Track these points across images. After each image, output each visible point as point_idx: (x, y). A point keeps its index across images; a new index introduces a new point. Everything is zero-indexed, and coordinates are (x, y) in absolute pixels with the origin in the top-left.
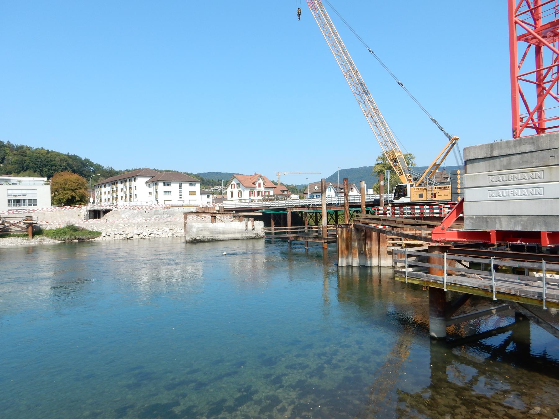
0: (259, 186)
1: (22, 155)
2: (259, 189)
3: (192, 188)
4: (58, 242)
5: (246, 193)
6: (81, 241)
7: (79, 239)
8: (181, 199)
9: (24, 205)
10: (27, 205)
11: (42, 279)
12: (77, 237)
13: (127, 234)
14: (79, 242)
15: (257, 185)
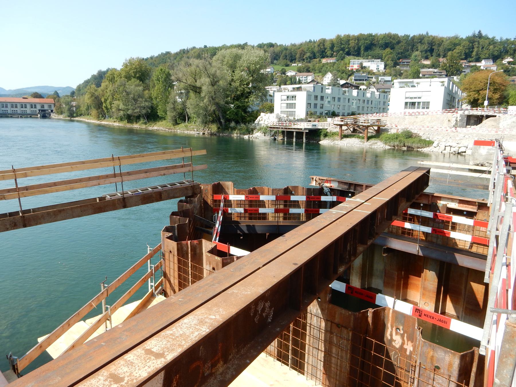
4: (387, 147)
6: (410, 149)
7: (408, 147)
9: (418, 108)
10: (421, 108)
12: (406, 144)
13: (460, 148)
14: (408, 150)
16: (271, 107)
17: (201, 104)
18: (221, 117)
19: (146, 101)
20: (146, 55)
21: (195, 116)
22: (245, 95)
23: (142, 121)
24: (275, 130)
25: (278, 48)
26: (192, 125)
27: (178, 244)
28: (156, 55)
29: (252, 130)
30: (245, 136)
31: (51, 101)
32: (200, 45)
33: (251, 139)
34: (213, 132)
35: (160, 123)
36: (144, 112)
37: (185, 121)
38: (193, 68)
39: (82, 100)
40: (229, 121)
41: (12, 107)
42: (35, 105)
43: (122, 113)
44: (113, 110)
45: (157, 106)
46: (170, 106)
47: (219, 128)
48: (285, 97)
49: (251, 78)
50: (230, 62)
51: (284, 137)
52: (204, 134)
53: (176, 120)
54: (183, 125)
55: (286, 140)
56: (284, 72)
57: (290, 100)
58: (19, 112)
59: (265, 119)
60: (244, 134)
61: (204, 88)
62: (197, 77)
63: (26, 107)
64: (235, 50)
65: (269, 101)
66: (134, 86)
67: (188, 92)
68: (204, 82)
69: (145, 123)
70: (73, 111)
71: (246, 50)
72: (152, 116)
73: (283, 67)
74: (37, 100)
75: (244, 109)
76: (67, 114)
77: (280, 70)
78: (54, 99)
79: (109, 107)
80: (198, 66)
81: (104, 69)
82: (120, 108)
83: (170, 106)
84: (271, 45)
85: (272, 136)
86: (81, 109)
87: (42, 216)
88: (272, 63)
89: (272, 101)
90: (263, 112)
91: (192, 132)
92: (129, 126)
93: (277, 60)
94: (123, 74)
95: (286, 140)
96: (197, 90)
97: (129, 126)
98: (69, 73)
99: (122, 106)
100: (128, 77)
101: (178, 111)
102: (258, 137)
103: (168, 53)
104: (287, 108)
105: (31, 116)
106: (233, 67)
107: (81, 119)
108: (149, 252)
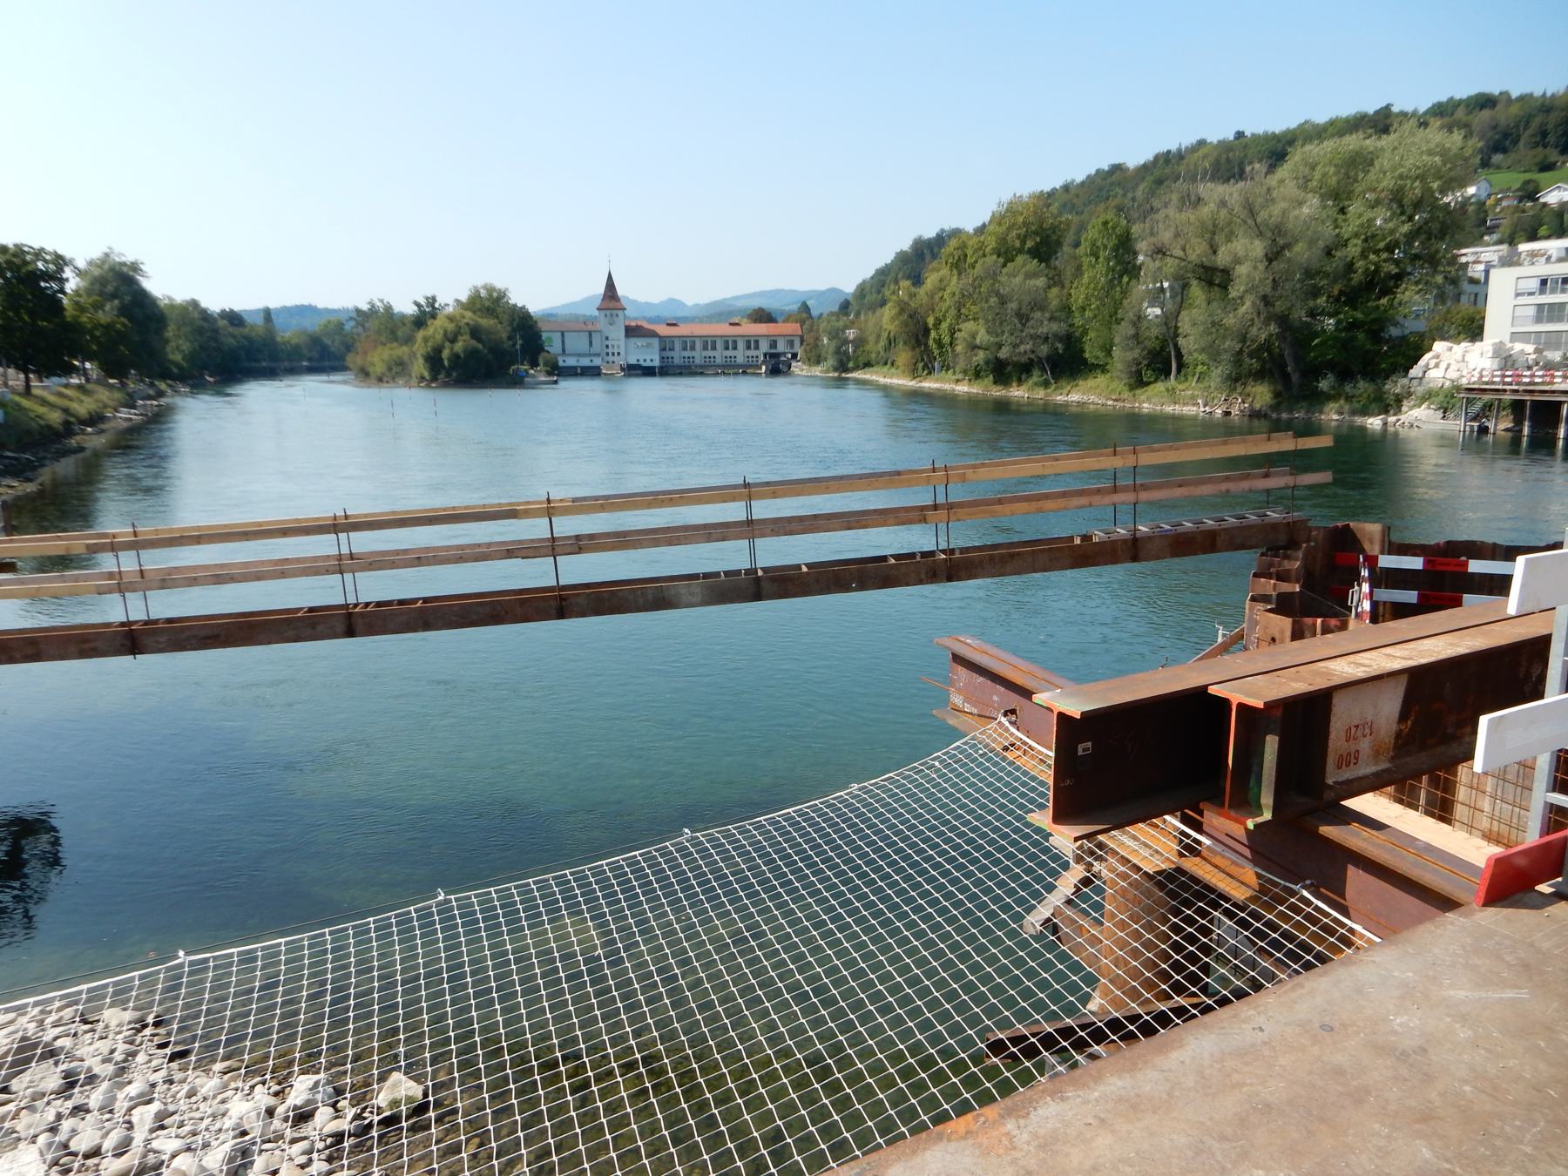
16: (1472, 320)
17: (1230, 320)
18: (1289, 360)
19: (1052, 319)
20: (1051, 181)
21: (1202, 357)
22: (1383, 285)
23: (1036, 376)
24: (1487, 397)
25: (1514, 110)
26: (1190, 387)
27: (1294, 623)
28: (1079, 178)
29: (1399, 401)
30: (1371, 420)
31: (793, 328)
32: (1219, 131)
33: (1391, 429)
34: (1257, 406)
35: (1091, 382)
36: (1044, 350)
37: (1167, 374)
38: (1206, 211)
39: (871, 324)
40: (1314, 372)
41: (705, 348)
42: (757, 342)
43: (981, 356)
44: (959, 349)
45: (1085, 332)
46: (1124, 330)
47: (1277, 395)
48: (1534, 284)
49: (1406, 228)
50: (1333, 181)
51: (1518, 422)
52: (1227, 414)
53: (1139, 373)
54: (1160, 386)
55: (1526, 431)
56: (1530, 193)
57: (1553, 291)
58: (740, 360)
59: (1451, 363)
60: (1365, 412)
61: (1242, 270)
62: (1219, 238)
63: (735, 348)
64: (1353, 142)
65: (1464, 299)
66: (1023, 278)
67: (1186, 286)
68: (1244, 253)
69: (1046, 384)
70: (846, 352)
71: (1393, 137)
72: (1068, 362)
73: (1528, 176)
74: (761, 329)
75: (1376, 329)
76: (831, 362)
77: (1517, 185)
78: (802, 322)
79: (947, 340)
80: (1223, 203)
81: (930, 233)
82: (978, 342)
83: (1124, 330)
84: (1485, 102)
85: (1474, 419)
86: (867, 348)
87: (981, 562)
88: (1485, 164)
89: (1480, 299)
90: (1443, 339)
91: (1189, 410)
92: (998, 392)
93: (1505, 151)
94: (991, 243)
95: (1526, 431)
96: (1216, 278)
97: (998, 392)
98: (833, 253)
99: (982, 337)
100: (1006, 254)
101: (1148, 344)
102: (1418, 420)
103: (1117, 168)
104: (1539, 319)
105: (746, 370)
106: (1339, 197)
107: (867, 377)
108: (1220, 640)
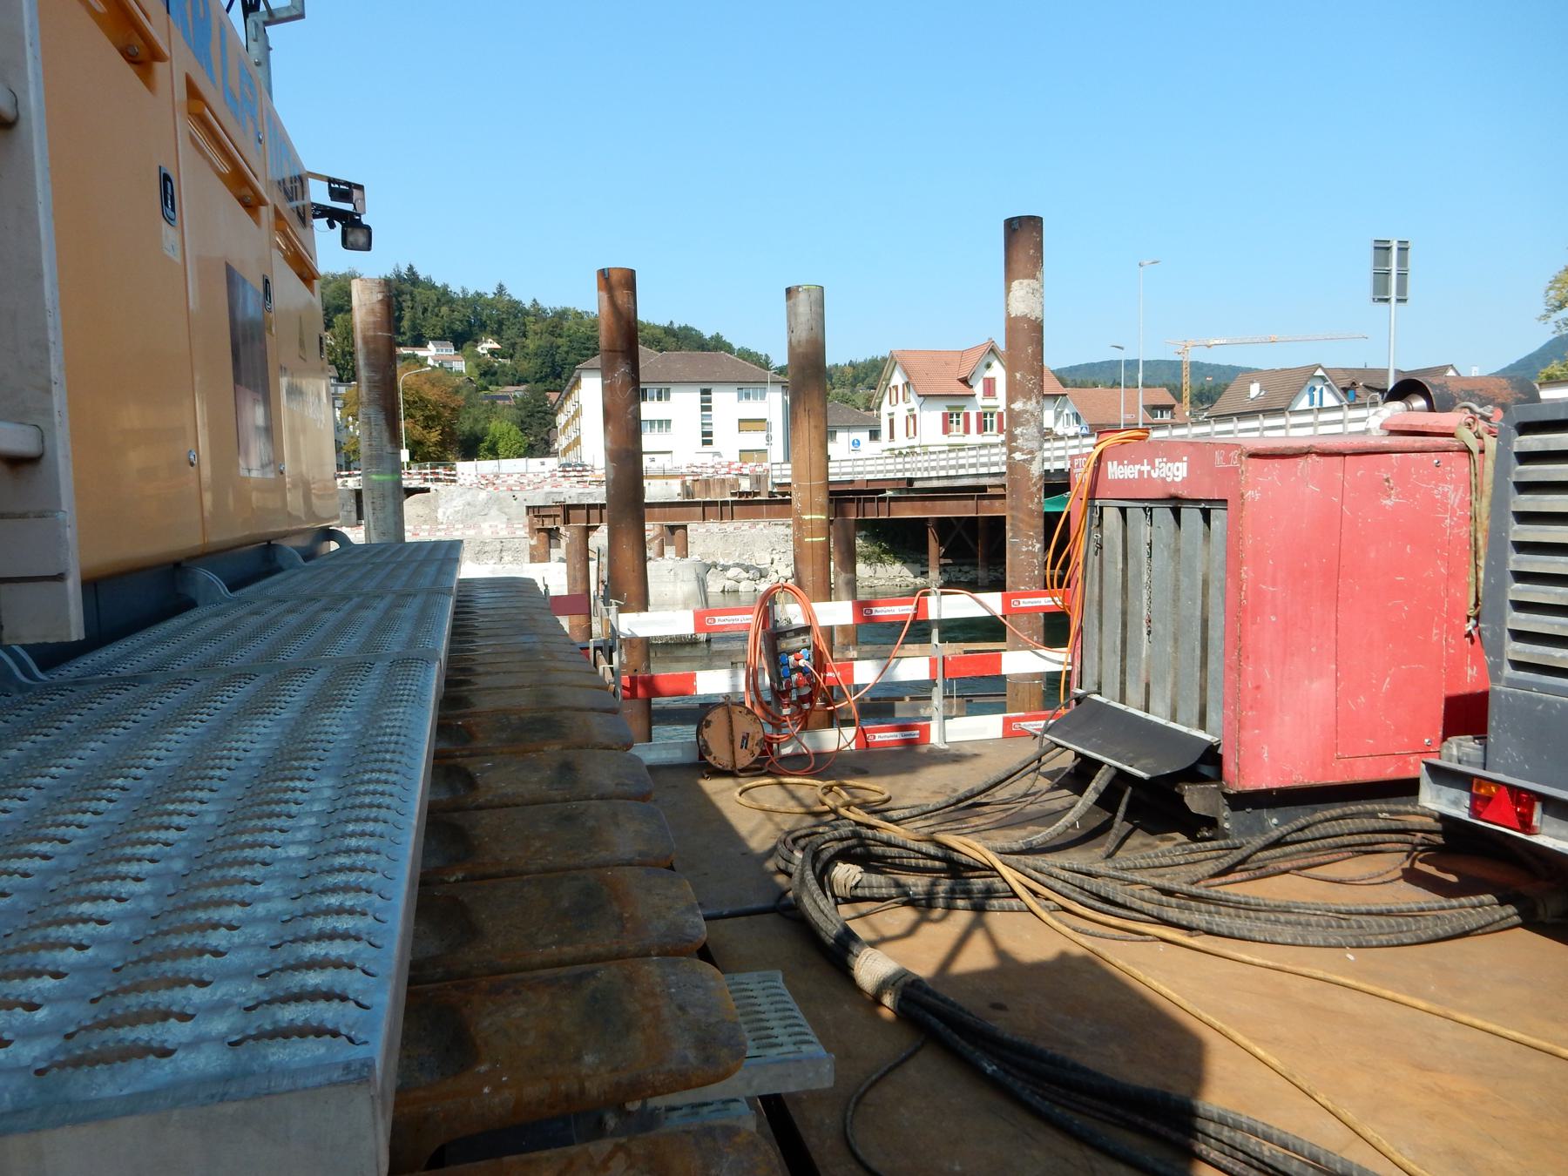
0: (989, 390)
1: (552, 333)
2: (989, 402)
3: (752, 408)
5: (931, 419)
8: (707, 448)
11: (975, 869)
15: (978, 389)
